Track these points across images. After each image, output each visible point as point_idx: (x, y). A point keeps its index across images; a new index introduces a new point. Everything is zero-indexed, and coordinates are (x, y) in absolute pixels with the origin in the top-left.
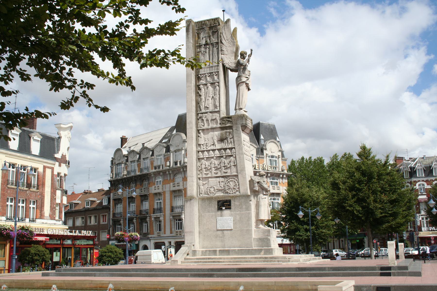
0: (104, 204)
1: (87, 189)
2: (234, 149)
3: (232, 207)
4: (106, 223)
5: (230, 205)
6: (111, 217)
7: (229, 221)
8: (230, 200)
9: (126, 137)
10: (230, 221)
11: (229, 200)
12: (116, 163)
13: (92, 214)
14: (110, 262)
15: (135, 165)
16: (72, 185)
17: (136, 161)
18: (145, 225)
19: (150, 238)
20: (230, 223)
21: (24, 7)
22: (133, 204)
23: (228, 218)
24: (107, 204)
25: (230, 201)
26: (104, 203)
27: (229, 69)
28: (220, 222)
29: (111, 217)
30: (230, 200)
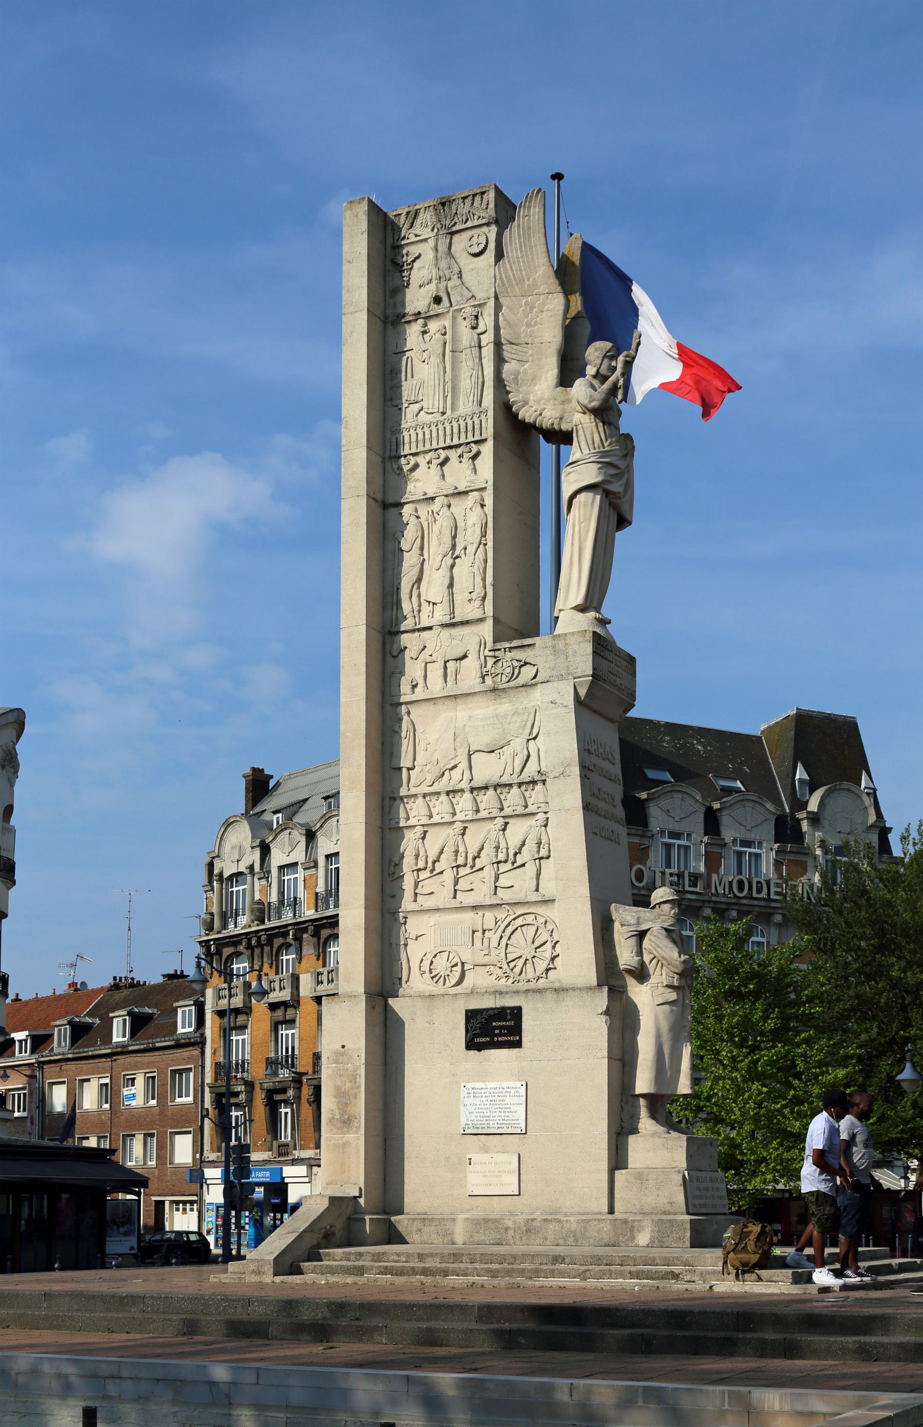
0: (180, 1030)
1: (122, 973)
2: (539, 787)
3: (527, 1036)
4: (190, 1099)
5: (517, 1030)
6: (208, 1079)
7: (508, 1100)
8: (519, 1009)
9: (248, 771)
10: (515, 1100)
11: (512, 1009)
12: (226, 874)
13: (137, 1067)
14: (789, 1070)
15: (296, 879)
16: (73, 959)
17: (300, 866)
18: (286, 1113)
19: (209, 1182)
20: (513, 1108)
21: (741, 760)
22: (290, 1032)
23: (505, 1084)
24: (191, 1030)
25: (517, 1013)
26: (183, 1027)
27: (541, 430)
28: (472, 1100)
29: (208, 1079)
30: (519, 1009)
